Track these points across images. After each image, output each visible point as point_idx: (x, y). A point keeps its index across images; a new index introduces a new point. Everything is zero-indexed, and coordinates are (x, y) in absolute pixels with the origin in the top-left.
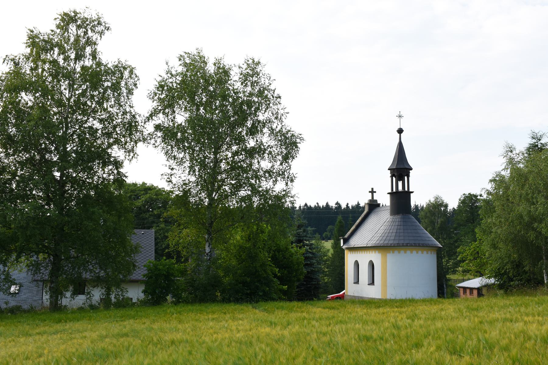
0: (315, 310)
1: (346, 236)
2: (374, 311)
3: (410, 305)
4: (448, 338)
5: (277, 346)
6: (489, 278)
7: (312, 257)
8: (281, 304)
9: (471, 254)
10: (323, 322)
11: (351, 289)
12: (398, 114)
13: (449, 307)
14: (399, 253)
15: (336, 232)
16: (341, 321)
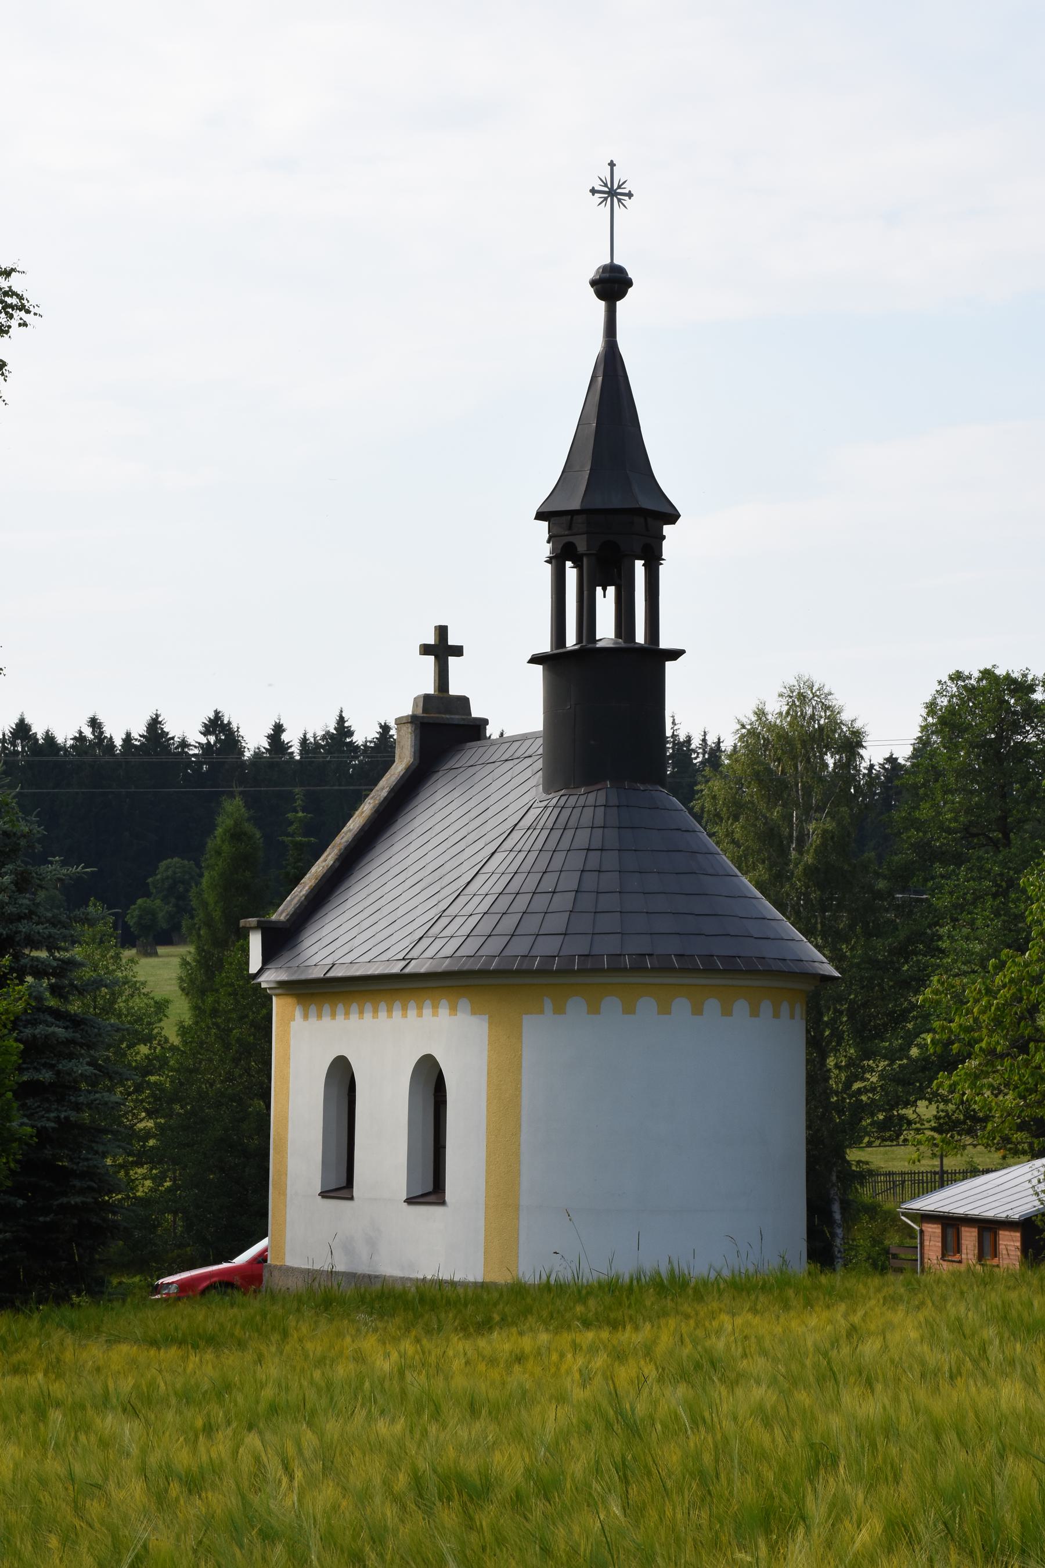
0: (95, 1352)
1: (282, 914)
2: (458, 1348)
3: (664, 1313)
4: (947, 1475)
9: (998, 1022)
11: (303, 1230)
12: (597, 174)
13: (889, 1325)
14: (594, 1009)
15: (210, 897)
16: (274, 1409)
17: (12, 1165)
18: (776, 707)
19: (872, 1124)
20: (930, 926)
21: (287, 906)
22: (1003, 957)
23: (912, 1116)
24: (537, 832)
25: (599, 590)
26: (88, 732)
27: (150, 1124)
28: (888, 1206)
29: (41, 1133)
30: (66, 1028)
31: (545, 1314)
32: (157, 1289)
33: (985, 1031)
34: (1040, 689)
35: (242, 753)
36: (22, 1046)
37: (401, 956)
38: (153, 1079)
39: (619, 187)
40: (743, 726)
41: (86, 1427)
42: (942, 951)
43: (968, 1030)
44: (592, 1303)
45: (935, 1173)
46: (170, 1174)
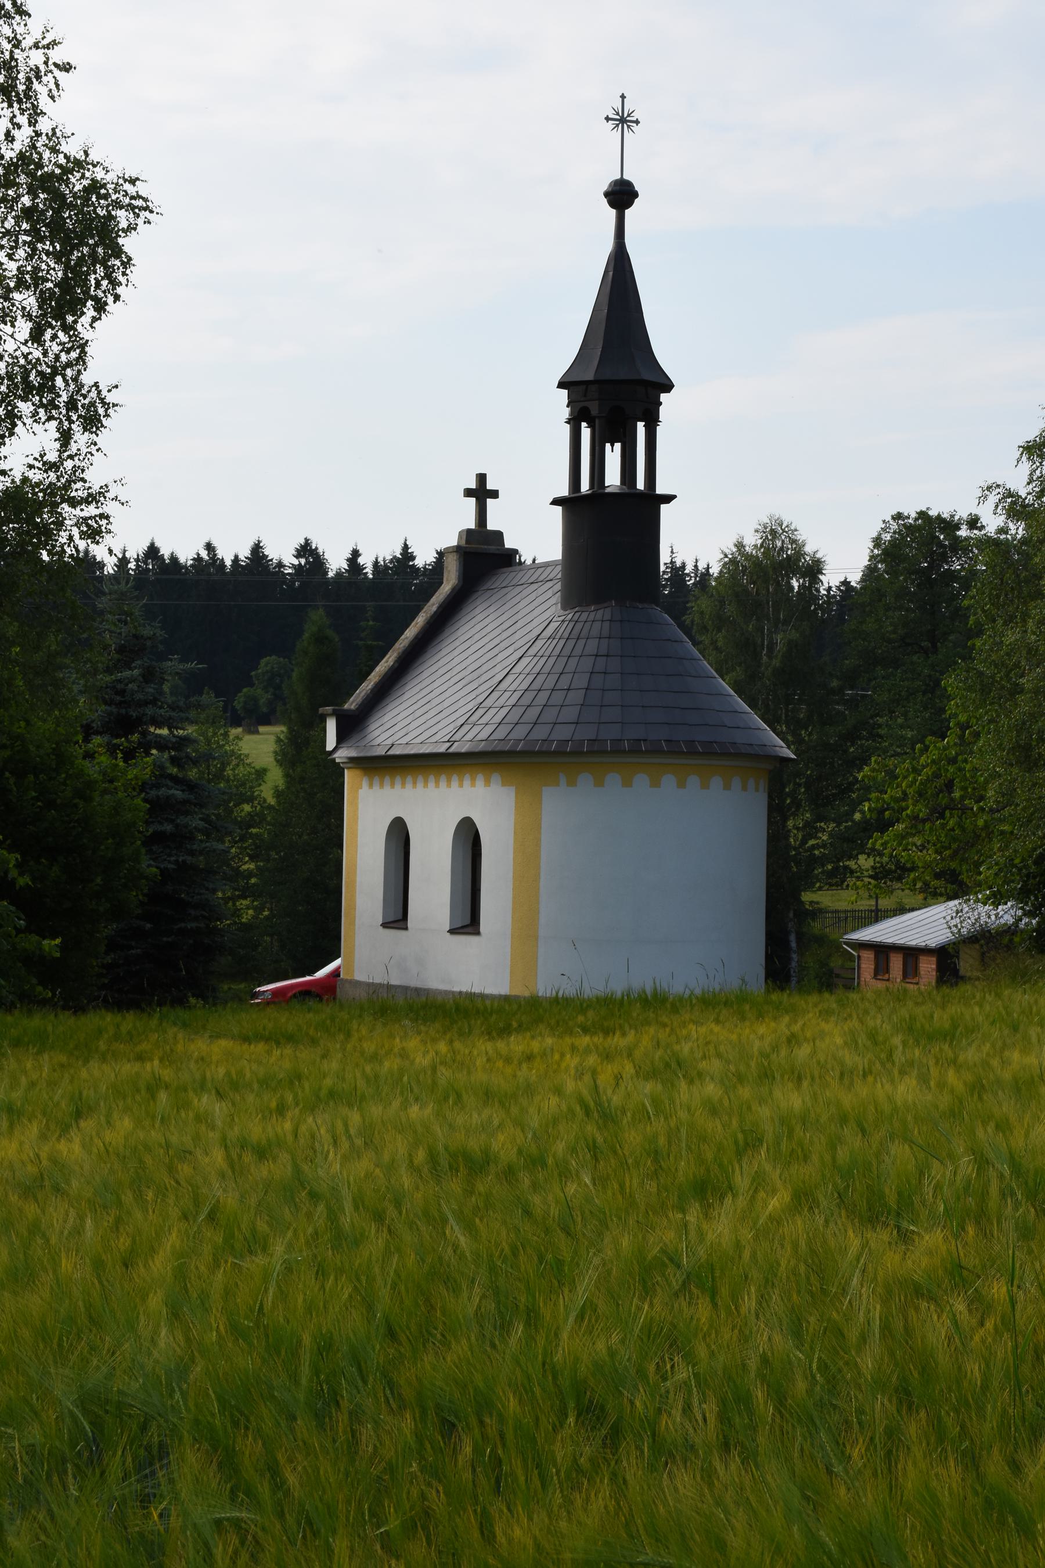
0: (200, 1046)
1: (352, 704)
2: (482, 1048)
3: (647, 1023)
4: (843, 1155)
5: (31, 1210)
6: (997, 899)
7: (189, 799)
8: (36, 1022)
9: (920, 794)
10: (251, 1098)
11: (367, 952)
13: (822, 1031)
14: (599, 783)
16: (332, 1094)
17: (141, 897)
18: (752, 540)
19: (823, 872)
20: (872, 717)
21: (357, 697)
22: (927, 743)
23: (854, 867)
24: (555, 641)
25: (608, 446)
26: (204, 554)
27: (252, 866)
28: (833, 937)
29: (163, 872)
30: (183, 791)
31: (553, 1022)
32: (255, 995)
33: (910, 801)
34: (964, 527)
35: (326, 573)
36: (148, 806)
37: (446, 739)
38: (254, 831)
39: (629, 115)
40: (726, 556)
41: (187, 1105)
42: (881, 737)
43: (897, 800)
44: (591, 1014)
45: (872, 911)
46: (268, 905)
